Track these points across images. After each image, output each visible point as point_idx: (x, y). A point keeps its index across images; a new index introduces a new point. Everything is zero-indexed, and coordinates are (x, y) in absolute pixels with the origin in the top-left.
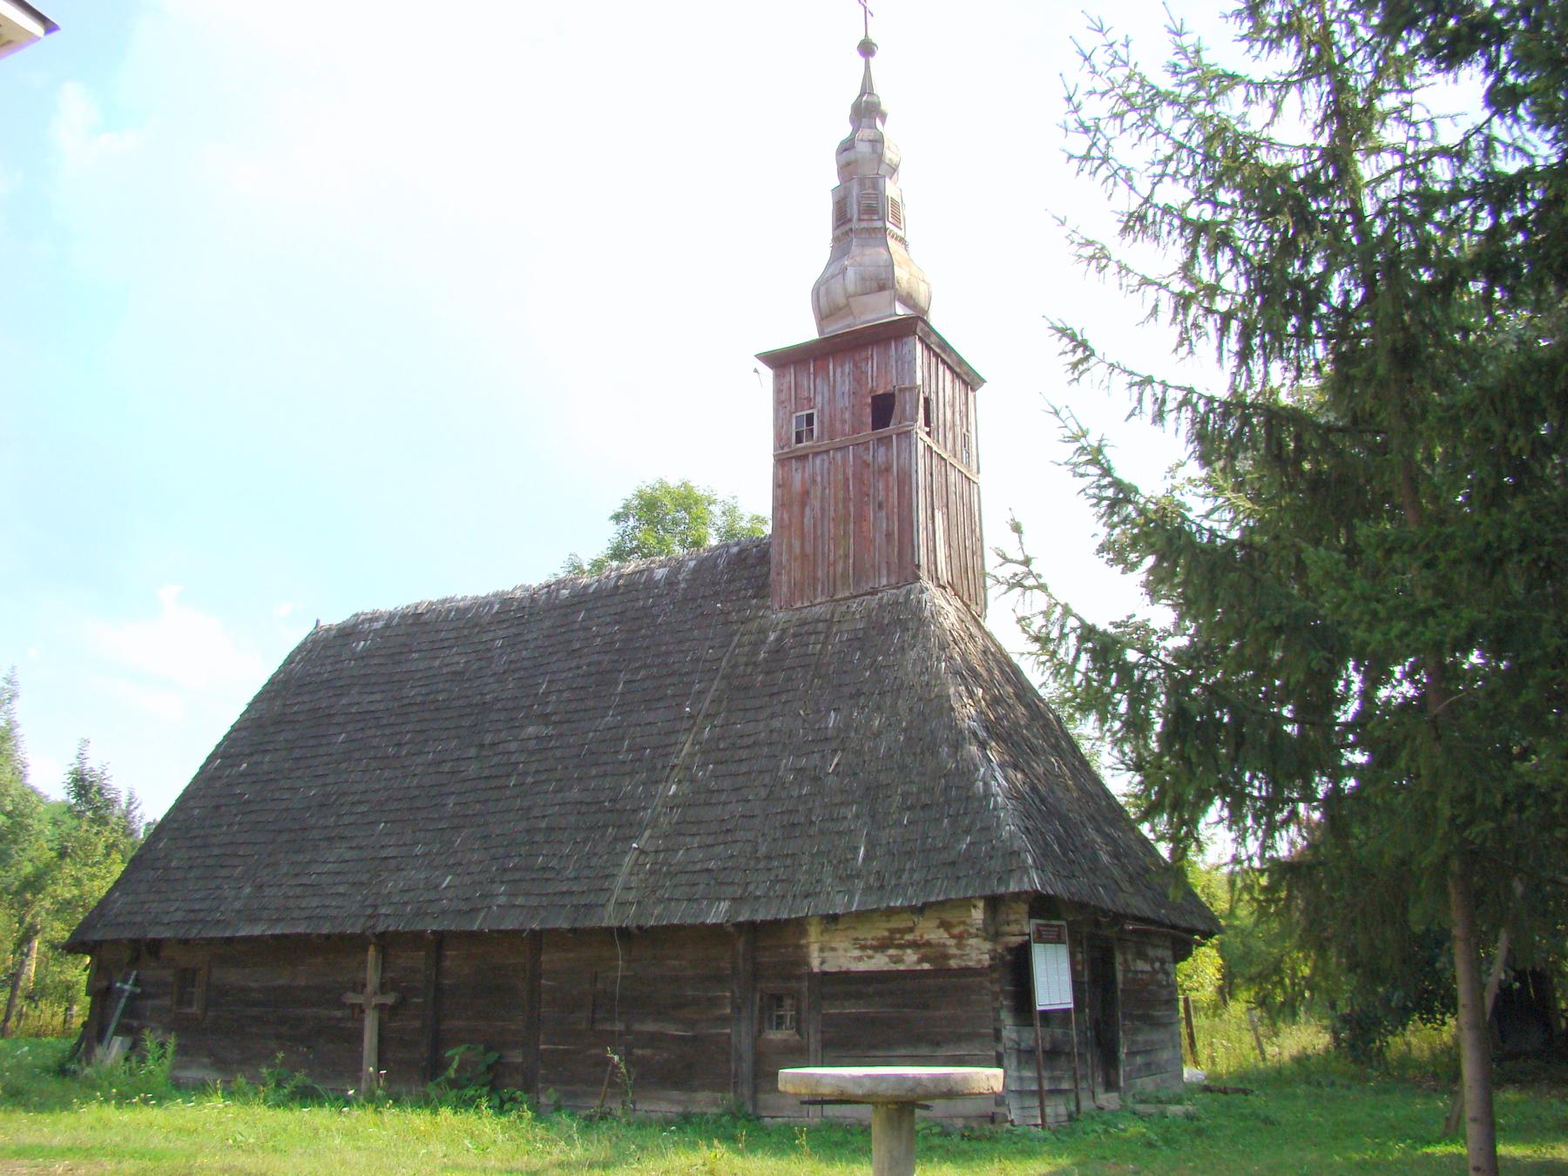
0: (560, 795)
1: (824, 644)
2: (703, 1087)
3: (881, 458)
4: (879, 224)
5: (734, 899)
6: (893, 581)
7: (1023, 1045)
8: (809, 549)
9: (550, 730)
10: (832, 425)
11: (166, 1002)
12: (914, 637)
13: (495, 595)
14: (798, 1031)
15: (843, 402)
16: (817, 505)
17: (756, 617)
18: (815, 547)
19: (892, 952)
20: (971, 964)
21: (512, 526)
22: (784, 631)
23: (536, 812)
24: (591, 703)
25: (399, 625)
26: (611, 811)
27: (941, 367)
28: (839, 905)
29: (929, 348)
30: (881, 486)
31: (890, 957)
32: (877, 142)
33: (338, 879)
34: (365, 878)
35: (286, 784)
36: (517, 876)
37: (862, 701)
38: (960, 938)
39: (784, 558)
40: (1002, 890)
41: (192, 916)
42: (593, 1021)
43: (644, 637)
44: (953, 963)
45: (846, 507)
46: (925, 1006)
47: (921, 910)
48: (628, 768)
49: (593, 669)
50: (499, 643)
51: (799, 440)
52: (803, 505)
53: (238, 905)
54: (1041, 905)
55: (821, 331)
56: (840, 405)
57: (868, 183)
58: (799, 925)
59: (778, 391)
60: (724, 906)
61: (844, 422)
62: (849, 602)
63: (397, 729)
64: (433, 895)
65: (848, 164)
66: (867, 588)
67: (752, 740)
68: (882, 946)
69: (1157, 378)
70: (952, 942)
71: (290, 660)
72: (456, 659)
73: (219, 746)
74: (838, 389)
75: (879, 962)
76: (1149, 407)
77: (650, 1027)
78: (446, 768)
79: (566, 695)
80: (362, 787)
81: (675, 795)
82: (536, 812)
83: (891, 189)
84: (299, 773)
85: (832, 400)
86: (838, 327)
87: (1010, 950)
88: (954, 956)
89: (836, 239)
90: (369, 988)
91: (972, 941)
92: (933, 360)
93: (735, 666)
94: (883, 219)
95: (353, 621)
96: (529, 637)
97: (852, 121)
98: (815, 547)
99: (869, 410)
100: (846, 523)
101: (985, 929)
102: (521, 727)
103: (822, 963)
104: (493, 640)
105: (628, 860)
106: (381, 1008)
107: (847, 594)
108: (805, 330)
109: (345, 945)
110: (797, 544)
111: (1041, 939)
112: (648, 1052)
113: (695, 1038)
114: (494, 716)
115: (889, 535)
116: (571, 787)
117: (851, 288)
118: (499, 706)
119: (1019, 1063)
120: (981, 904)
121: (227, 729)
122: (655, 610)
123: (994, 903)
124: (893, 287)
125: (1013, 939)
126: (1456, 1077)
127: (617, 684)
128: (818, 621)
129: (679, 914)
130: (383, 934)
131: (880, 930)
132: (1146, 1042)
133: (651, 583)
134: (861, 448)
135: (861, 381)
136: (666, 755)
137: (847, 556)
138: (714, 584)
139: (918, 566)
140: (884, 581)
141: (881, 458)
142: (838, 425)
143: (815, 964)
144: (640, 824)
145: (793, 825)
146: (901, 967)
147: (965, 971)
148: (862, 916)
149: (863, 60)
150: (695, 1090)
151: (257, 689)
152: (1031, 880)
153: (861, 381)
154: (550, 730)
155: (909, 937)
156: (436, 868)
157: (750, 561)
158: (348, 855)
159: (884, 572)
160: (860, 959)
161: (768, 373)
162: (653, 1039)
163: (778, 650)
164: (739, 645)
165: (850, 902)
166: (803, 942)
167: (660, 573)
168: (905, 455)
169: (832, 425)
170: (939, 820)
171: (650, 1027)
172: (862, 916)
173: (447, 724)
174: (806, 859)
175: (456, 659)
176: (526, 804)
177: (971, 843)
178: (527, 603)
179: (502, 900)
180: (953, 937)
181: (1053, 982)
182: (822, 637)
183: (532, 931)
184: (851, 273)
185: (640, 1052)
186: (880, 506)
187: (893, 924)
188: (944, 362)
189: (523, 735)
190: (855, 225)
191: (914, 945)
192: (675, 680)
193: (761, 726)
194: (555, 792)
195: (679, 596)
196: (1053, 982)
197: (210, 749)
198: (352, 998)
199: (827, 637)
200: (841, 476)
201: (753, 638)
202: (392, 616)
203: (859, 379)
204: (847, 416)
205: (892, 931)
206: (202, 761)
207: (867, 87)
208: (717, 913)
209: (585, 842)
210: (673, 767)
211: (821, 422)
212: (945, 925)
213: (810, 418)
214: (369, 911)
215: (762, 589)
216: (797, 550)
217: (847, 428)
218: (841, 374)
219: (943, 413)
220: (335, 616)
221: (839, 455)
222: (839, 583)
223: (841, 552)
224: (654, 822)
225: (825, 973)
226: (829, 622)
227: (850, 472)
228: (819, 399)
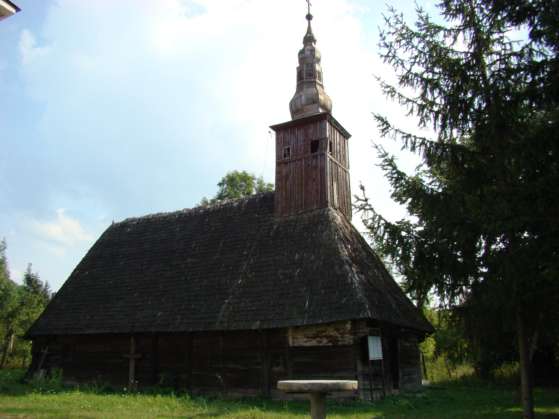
1: (294, 229)
3: (314, 163)
4: (313, 80)
6: (318, 207)
8: (288, 196)
9: (196, 260)
14: (285, 367)
15: (301, 143)
16: (291, 180)
19: (318, 339)
22: (279, 225)
25: (142, 223)
27: (335, 131)
28: (299, 322)
29: (331, 124)
30: (314, 173)
31: (317, 341)
32: (313, 50)
37: (307, 250)
38: (342, 334)
44: (340, 343)
47: (328, 324)
50: (178, 229)
51: (285, 157)
52: (286, 180)
54: (371, 322)
57: (309, 65)
58: (285, 330)
59: (277, 139)
60: (258, 323)
61: (301, 150)
62: (303, 215)
65: (302, 58)
66: (309, 210)
68: (314, 337)
69: (413, 135)
70: (340, 336)
72: (162, 235)
73: (78, 266)
74: (299, 138)
75: (314, 343)
76: (409, 145)
81: (241, 283)
83: (317, 67)
85: (297, 142)
86: (299, 117)
88: (340, 341)
89: (298, 85)
91: (347, 335)
92: (333, 128)
94: (315, 78)
99: (310, 146)
103: (293, 343)
104: (176, 228)
106: (135, 359)
107: (302, 212)
108: (287, 118)
110: (284, 194)
111: (371, 335)
115: (317, 191)
119: (363, 379)
123: (355, 322)
124: (318, 102)
125: (361, 334)
126: (519, 383)
129: (242, 326)
131: (310, 333)
133: (232, 208)
134: (307, 160)
135: (308, 135)
137: (302, 198)
139: (327, 202)
140: (315, 207)
141: (314, 163)
142: (299, 151)
145: (283, 294)
146: (321, 345)
147: (344, 346)
148: (308, 327)
152: (368, 314)
153: (308, 135)
154: (196, 260)
155: (324, 334)
159: (315, 204)
160: (307, 342)
161: (274, 133)
163: (277, 231)
164: (263, 230)
165: (303, 321)
166: (286, 336)
167: (235, 204)
168: (322, 162)
172: (308, 327)
179: (179, 321)
180: (339, 334)
183: (190, 332)
184: (303, 97)
185: (228, 375)
186: (314, 180)
187: (318, 329)
188: (337, 129)
190: (305, 80)
191: (326, 337)
198: (125, 356)
199: (295, 227)
200: (300, 170)
202: (140, 219)
203: (306, 135)
204: (302, 148)
206: (72, 271)
207: (309, 30)
208: (256, 325)
210: (240, 273)
211: (293, 150)
212: (337, 330)
213: (289, 149)
215: (272, 210)
218: (300, 133)
219: (337, 147)
220: (120, 220)
221: (299, 162)
222: (299, 208)
223: (300, 196)
225: (294, 347)
227: (303, 168)
228: (292, 142)
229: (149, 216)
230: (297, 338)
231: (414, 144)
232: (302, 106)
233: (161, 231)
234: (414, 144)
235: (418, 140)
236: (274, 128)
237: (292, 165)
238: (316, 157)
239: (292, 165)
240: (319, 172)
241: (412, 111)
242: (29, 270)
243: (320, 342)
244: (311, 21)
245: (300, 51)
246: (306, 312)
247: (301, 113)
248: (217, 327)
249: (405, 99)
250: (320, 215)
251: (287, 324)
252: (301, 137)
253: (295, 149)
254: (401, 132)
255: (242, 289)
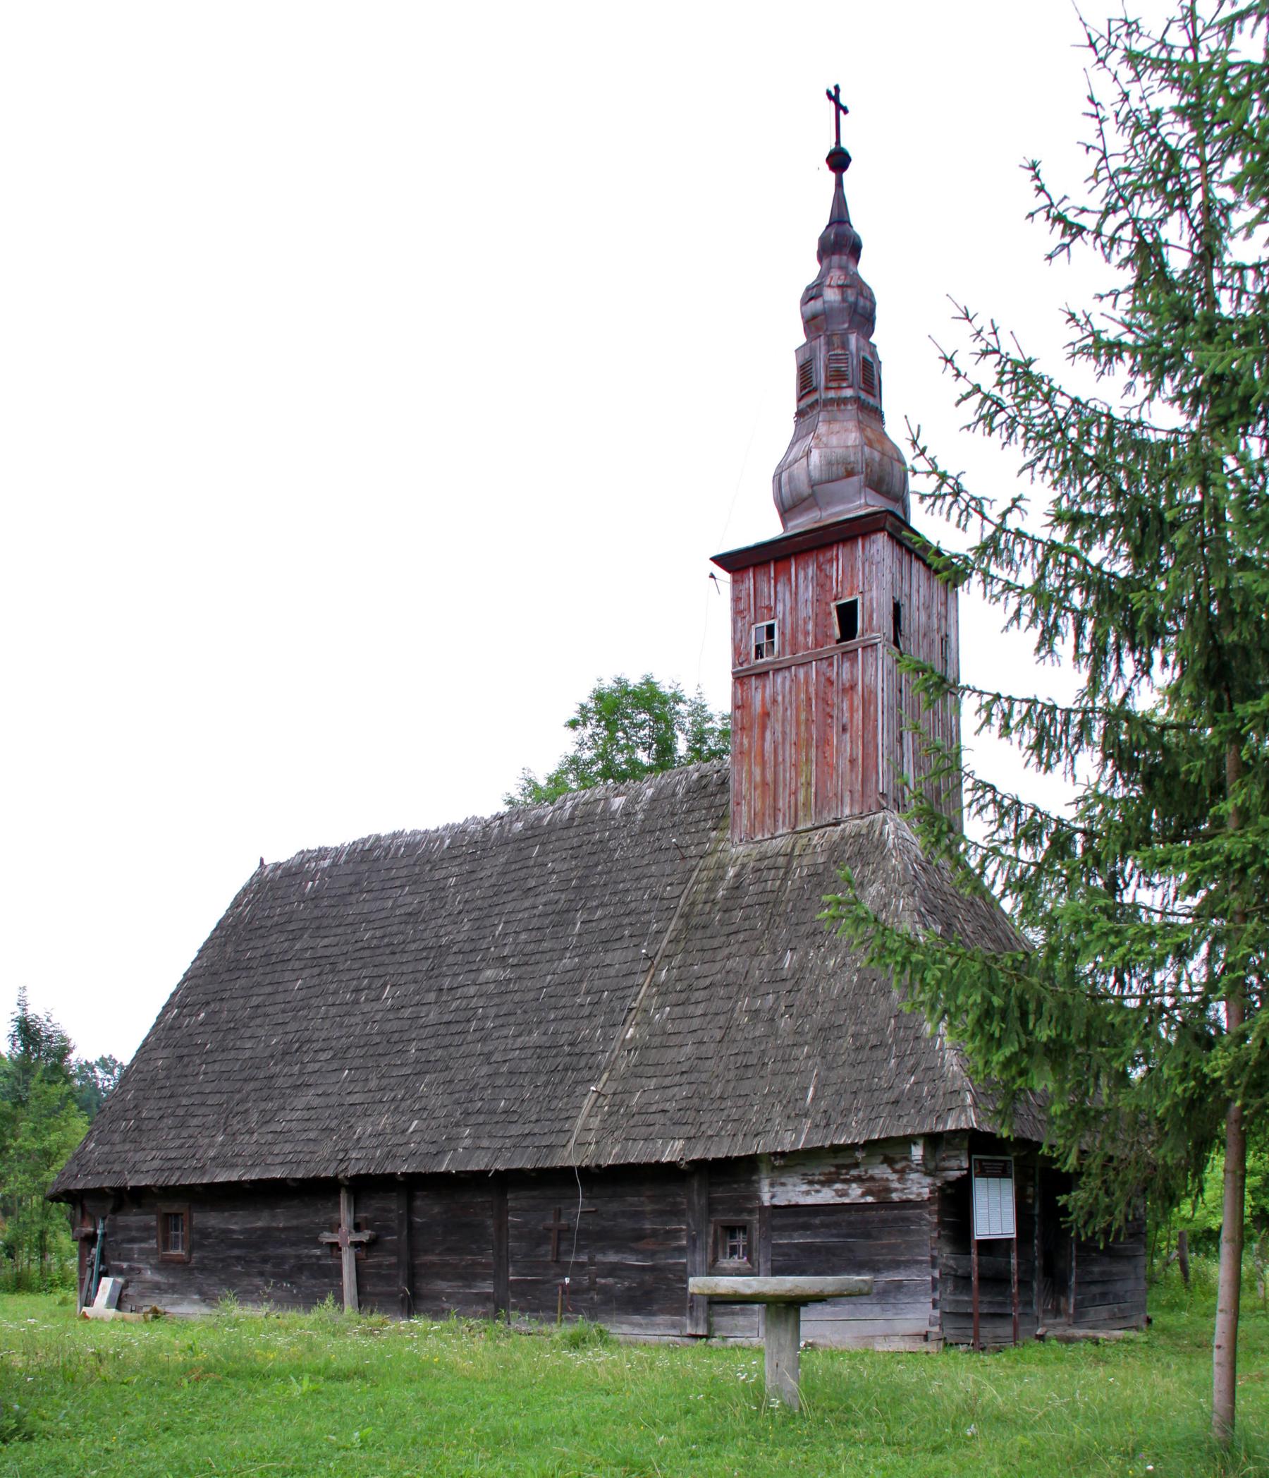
0: (520, 1040)
1: (784, 879)
2: (662, 1312)
3: (846, 676)
5: (689, 1139)
6: (856, 811)
7: (960, 1272)
8: (769, 777)
9: (508, 973)
10: (794, 637)
11: (153, 1244)
12: (873, 873)
13: (446, 828)
14: (749, 1260)
16: (779, 728)
17: (715, 851)
18: (776, 774)
19: (838, 1186)
20: (911, 1197)
21: (461, 750)
22: (744, 866)
23: (497, 1057)
24: (546, 945)
25: (346, 862)
26: (569, 1055)
30: (845, 706)
31: (836, 1191)
33: (308, 1124)
34: (333, 1125)
35: (248, 1033)
36: (481, 1119)
37: (819, 939)
39: (745, 786)
40: (940, 1128)
41: (168, 1164)
42: (558, 1253)
43: (600, 874)
44: (895, 1196)
45: (808, 729)
46: (868, 1236)
48: (586, 1011)
49: (550, 909)
50: (452, 881)
51: (757, 658)
52: (763, 728)
53: (212, 1153)
54: (977, 1142)
55: (785, 531)
56: (802, 614)
59: (736, 599)
61: (806, 634)
63: (354, 974)
64: (402, 1140)
66: (830, 819)
67: (708, 981)
69: (1004, 694)
70: (895, 1177)
71: (236, 903)
72: (409, 899)
73: (173, 995)
75: (826, 1196)
76: (997, 722)
77: (612, 1258)
78: (406, 1013)
79: (523, 937)
80: (324, 1035)
81: (632, 1038)
82: (497, 1057)
84: (258, 1021)
85: (794, 609)
86: (804, 522)
87: (949, 1184)
88: (896, 1190)
89: (800, 414)
90: (344, 1228)
91: (913, 1176)
92: (906, 558)
93: (693, 904)
95: (298, 861)
96: (482, 874)
97: (820, 259)
98: (776, 774)
100: (808, 746)
101: (924, 1164)
102: (479, 970)
103: (772, 1197)
104: (446, 878)
105: (587, 1104)
106: (356, 1245)
107: (809, 826)
108: (766, 526)
109: (318, 1190)
110: (757, 771)
111: (984, 1173)
112: (610, 1280)
113: (652, 1269)
114: (450, 959)
115: (852, 761)
116: (530, 1033)
117: (816, 474)
118: (455, 949)
119: (956, 1288)
120: (921, 1142)
121: (180, 977)
122: (612, 844)
125: (951, 1173)
127: (575, 924)
128: (778, 854)
129: (637, 1154)
130: (358, 1177)
132: (1103, 1273)
134: (825, 663)
136: (624, 998)
137: (809, 784)
138: (673, 815)
140: (847, 812)
141: (846, 676)
142: (801, 638)
143: (766, 1199)
144: (598, 1067)
145: (746, 1066)
146: (847, 1200)
147: (906, 1203)
149: (832, 176)
150: (653, 1314)
151: (206, 935)
152: (968, 1119)
154: (508, 973)
155: (854, 1172)
156: (403, 1113)
157: (711, 789)
158: (316, 1102)
159: (847, 799)
160: (808, 1193)
161: (725, 577)
162: (613, 1270)
163: (737, 887)
164: (697, 882)
165: (798, 1139)
166: (754, 1178)
169: (794, 637)
170: (886, 1060)
171: (612, 1258)
173: (405, 968)
174: (757, 1099)
175: (409, 899)
176: (486, 1050)
177: (916, 1083)
178: (478, 837)
179: (467, 1142)
180: (895, 1171)
181: (994, 1213)
182: (782, 872)
183: (497, 1171)
184: (815, 457)
185: (603, 1281)
186: (844, 729)
187: (839, 1161)
189: (481, 979)
191: (859, 1180)
192: (632, 919)
193: (718, 966)
194: (516, 1037)
195: (636, 829)
196: (994, 1213)
197: (165, 999)
198: (327, 1237)
199: (786, 873)
200: (803, 696)
201: (712, 874)
202: (338, 852)
203: (822, 585)
204: (810, 627)
205: (837, 1167)
206: (159, 1010)
209: (545, 1085)
210: (631, 1010)
213: (770, 629)
214: (341, 1156)
215: (721, 820)
216: (758, 778)
217: (810, 639)
218: (804, 576)
220: (282, 852)
221: (801, 672)
222: (801, 814)
223: (803, 780)
224: (611, 1066)
225: (775, 1207)
226: (789, 856)
227: (812, 690)
228: (780, 607)
229: (364, 841)
230: (783, 1184)
231: (1007, 716)
232: (813, 484)
233: (402, 887)
234: (1007, 716)
235: (1017, 706)
236: (721, 560)
237: (779, 680)
238: (850, 654)
239: (779, 680)
240: (858, 701)
241: (1017, 615)
242: (23, 1005)
243: (843, 1194)
244: (846, 176)
245: (808, 289)
246: (806, 1116)
247: (808, 509)
248: (569, 1157)
249: (1001, 583)
250: (859, 835)
251: (758, 1146)
252: (808, 592)
253: (788, 631)
254: (974, 691)
255: (634, 1057)
